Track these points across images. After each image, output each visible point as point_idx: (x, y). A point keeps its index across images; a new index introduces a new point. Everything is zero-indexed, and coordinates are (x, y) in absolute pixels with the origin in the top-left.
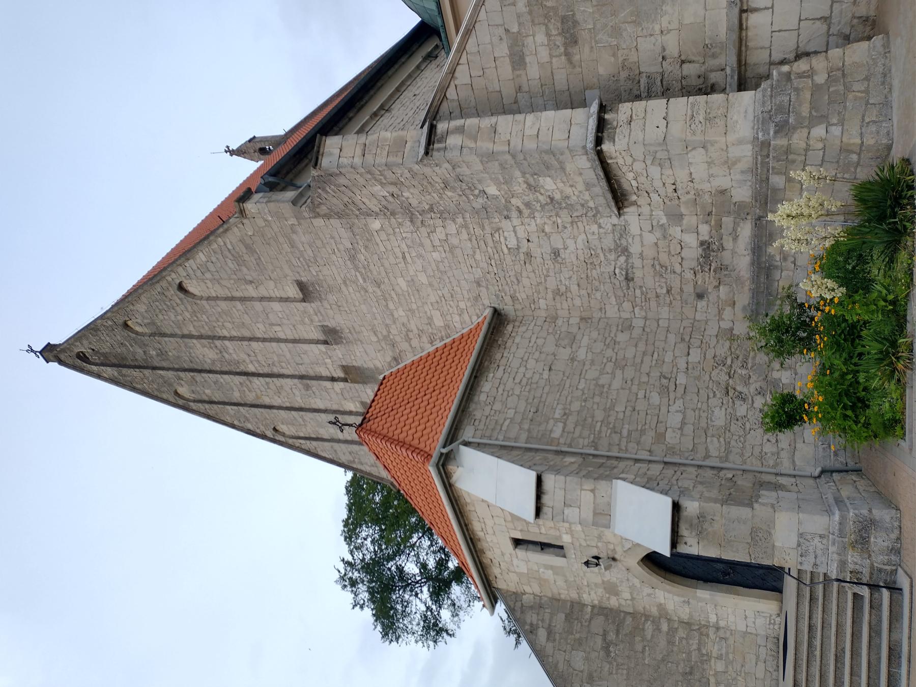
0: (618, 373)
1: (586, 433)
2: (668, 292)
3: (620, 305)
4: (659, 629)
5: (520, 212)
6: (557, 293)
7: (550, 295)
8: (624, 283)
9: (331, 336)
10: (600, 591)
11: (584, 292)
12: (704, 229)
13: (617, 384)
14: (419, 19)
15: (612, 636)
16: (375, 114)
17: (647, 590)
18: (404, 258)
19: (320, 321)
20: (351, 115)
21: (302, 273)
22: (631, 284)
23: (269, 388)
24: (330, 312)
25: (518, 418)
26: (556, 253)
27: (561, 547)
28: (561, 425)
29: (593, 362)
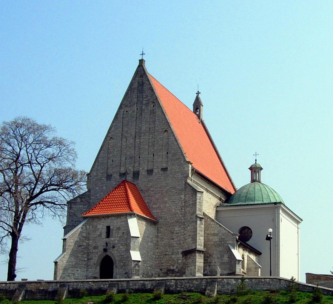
2: (162, 263)
3: (159, 252)
5: (183, 232)
6: (163, 238)
8: (165, 254)
11: (163, 244)
12: (177, 270)
14: (232, 194)
15: (82, 247)
18: (173, 202)
19: (155, 171)
20: (207, 182)
21: (170, 172)
22: (164, 255)
23: (130, 144)
24: (158, 176)
29: (148, 246)
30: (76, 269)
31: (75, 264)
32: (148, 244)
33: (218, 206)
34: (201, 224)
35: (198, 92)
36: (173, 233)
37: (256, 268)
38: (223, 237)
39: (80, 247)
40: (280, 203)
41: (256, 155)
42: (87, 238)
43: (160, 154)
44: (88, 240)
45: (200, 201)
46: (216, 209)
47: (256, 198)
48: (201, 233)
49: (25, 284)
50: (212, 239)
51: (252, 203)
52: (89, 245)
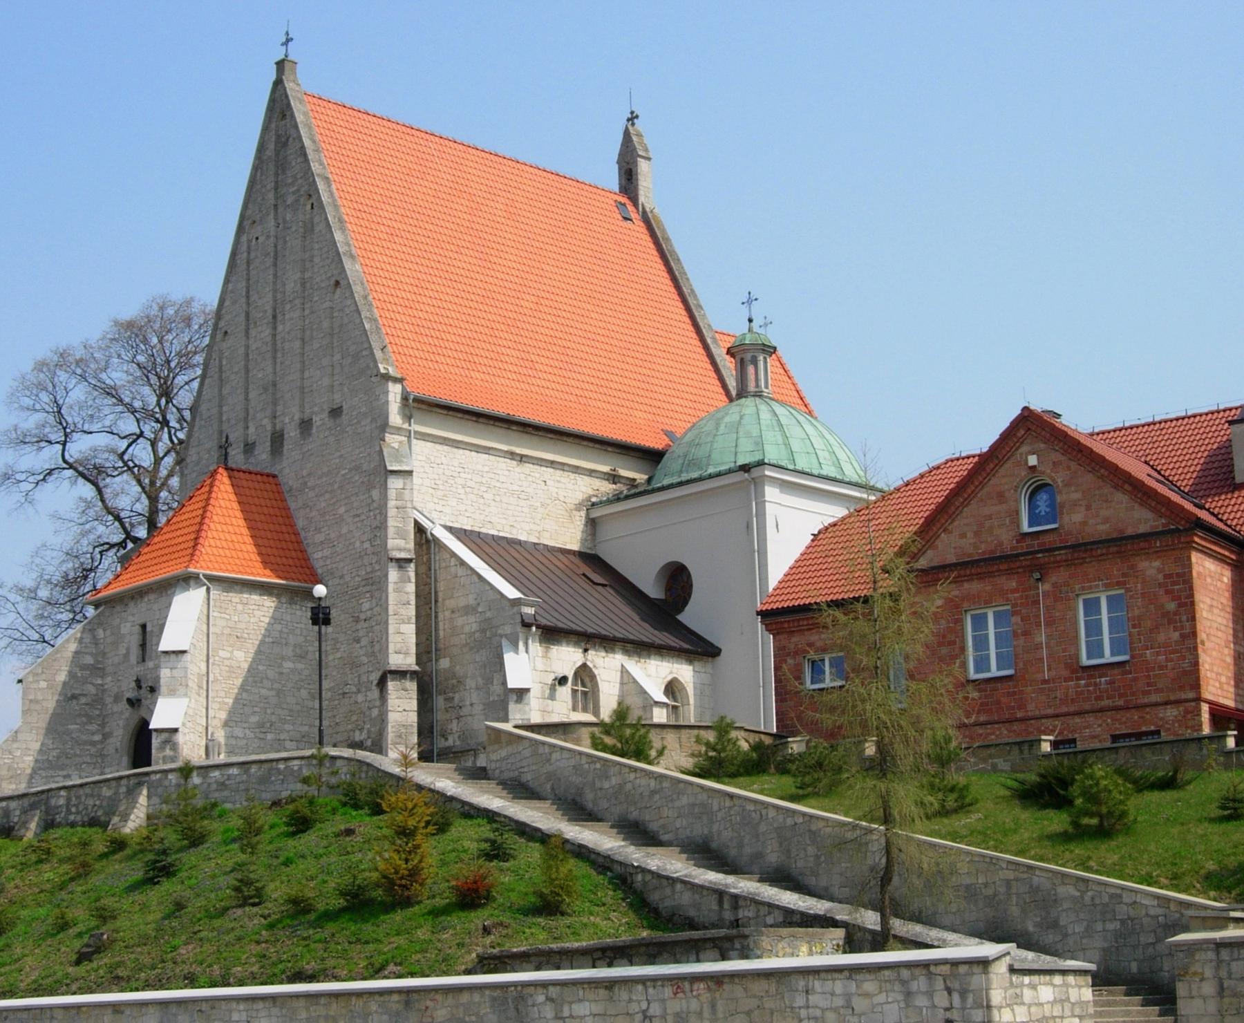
0: (274, 693)
1: (224, 674)
4: (93, 734)
7: (334, 636)
9: (306, 425)
10: (116, 690)
13: (264, 692)
15: (83, 700)
16: (512, 455)
17: (121, 723)
25: (231, 624)
26: (358, 641)
27: (144, 660)
28: (228, 655)
30: (65, 773)
31: (58, 758)
32: (280, 666)
33: (593, 504)
34: (404, 582)
35: (632, 113)
36: (357, 620)
37: (644, 707)
38: (489, 614)
39: (75, 702)
40: (761, 464)
41: (750, 301)
42: (97, 669)
43: (325, 362)
44: (102, 677)
45: (399, 503)
46: (588, 514)
47: (713, 456)
48: (402, 611)
49: (801, 792)
50: (463, 627)
51: (695, 475)
52: (104, 691)
